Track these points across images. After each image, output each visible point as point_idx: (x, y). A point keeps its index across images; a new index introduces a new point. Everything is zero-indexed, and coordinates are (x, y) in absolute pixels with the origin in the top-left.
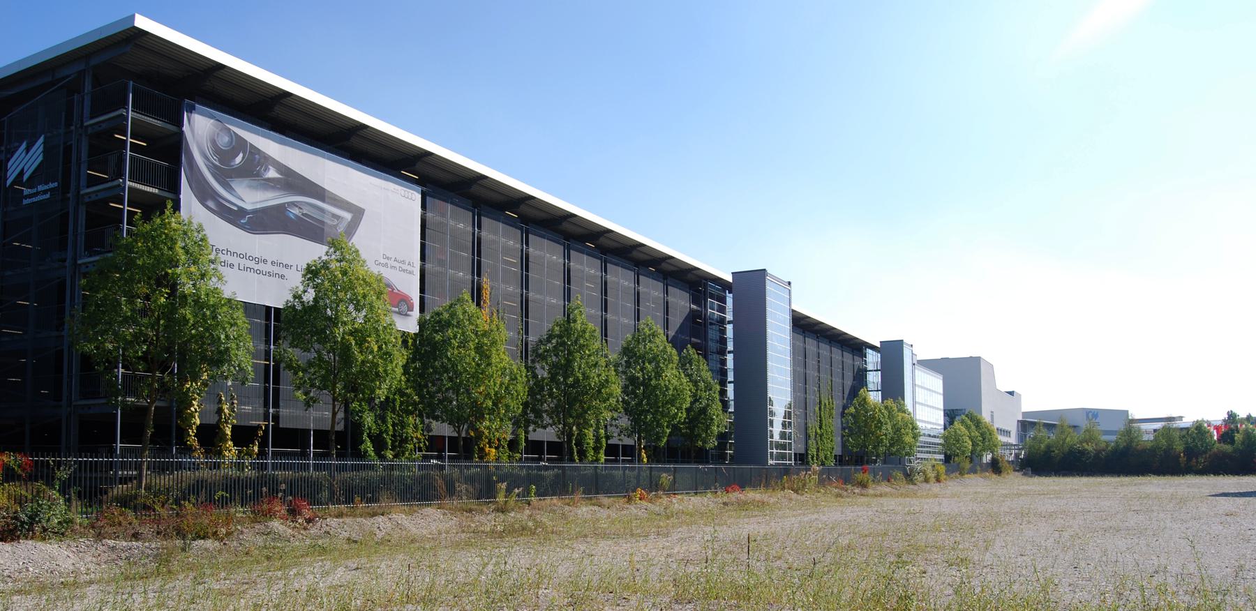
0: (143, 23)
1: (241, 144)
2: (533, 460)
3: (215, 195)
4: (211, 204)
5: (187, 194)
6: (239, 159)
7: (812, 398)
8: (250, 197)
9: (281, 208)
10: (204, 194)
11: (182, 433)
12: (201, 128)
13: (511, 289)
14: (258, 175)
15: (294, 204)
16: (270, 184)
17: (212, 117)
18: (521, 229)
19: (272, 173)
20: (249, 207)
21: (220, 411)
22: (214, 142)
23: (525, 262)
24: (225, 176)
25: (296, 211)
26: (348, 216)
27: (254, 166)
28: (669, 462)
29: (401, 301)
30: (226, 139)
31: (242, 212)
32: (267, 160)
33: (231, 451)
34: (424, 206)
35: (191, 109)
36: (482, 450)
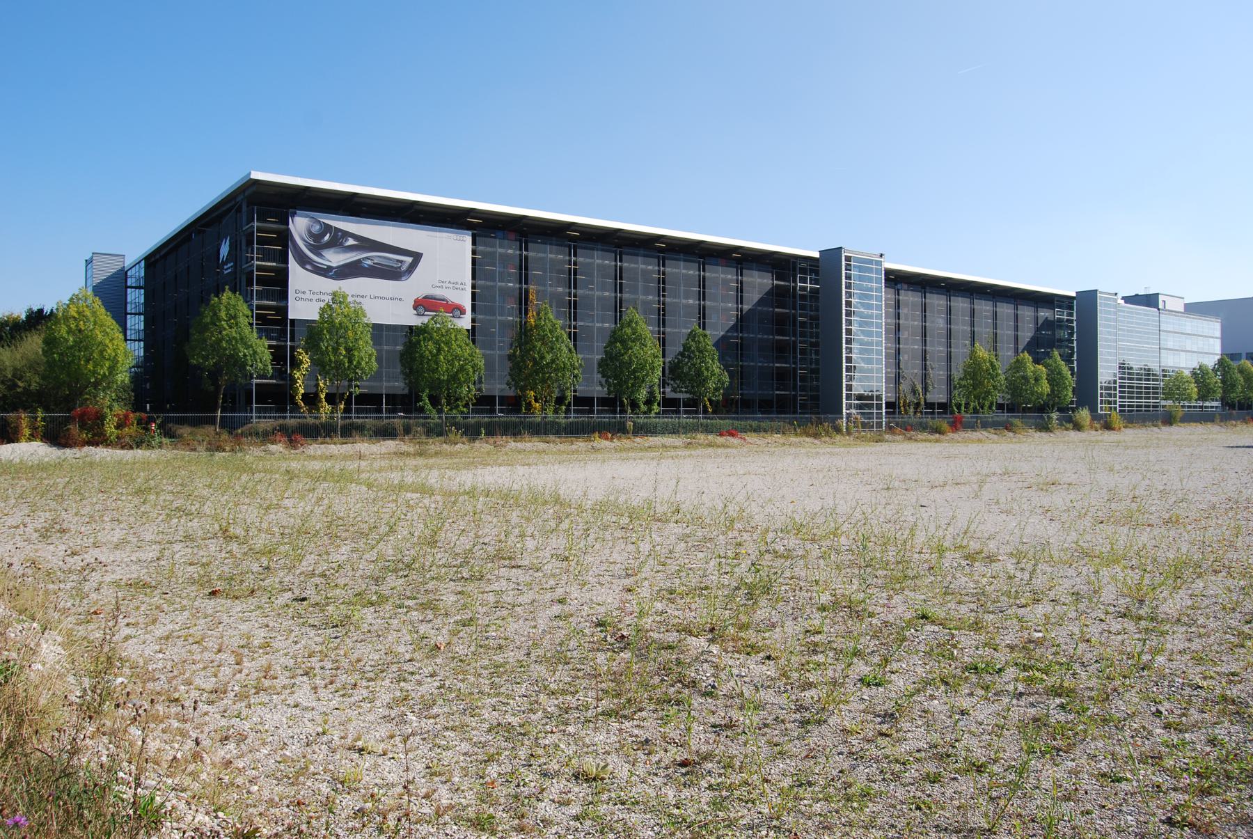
0: (256, 175)
1: (328, 228)
2: (607, 411)
3: (310, 261)
4: (308, 267)
5: (293, 265)
6: (327, 238)
7: (911, 346)
8: (334, 258)
9: (359, 261)
10: (303, 261)
11: (293, 397)
12: (300, 225)
13: (691, 301)
14: (341, 244)
15: (367, 258)
16: (351, 248)
17: (307, 216)
18: (658, 257)
19: (351, 242)
20: (334, 265)
21: (317, 385)
22: (310, 232)
23: (995, 314)
24: (317, 248)
25: (369, 262)
26: (409, 260)
27: (338, 240)
28: (841, 413)
29: (457, 310)
30: (318, 227)
31: (330, 268)
32: (347, 234)
33: (326, 407)
34: (474, 243)
35: (294, 215)
36: (529, 404)
